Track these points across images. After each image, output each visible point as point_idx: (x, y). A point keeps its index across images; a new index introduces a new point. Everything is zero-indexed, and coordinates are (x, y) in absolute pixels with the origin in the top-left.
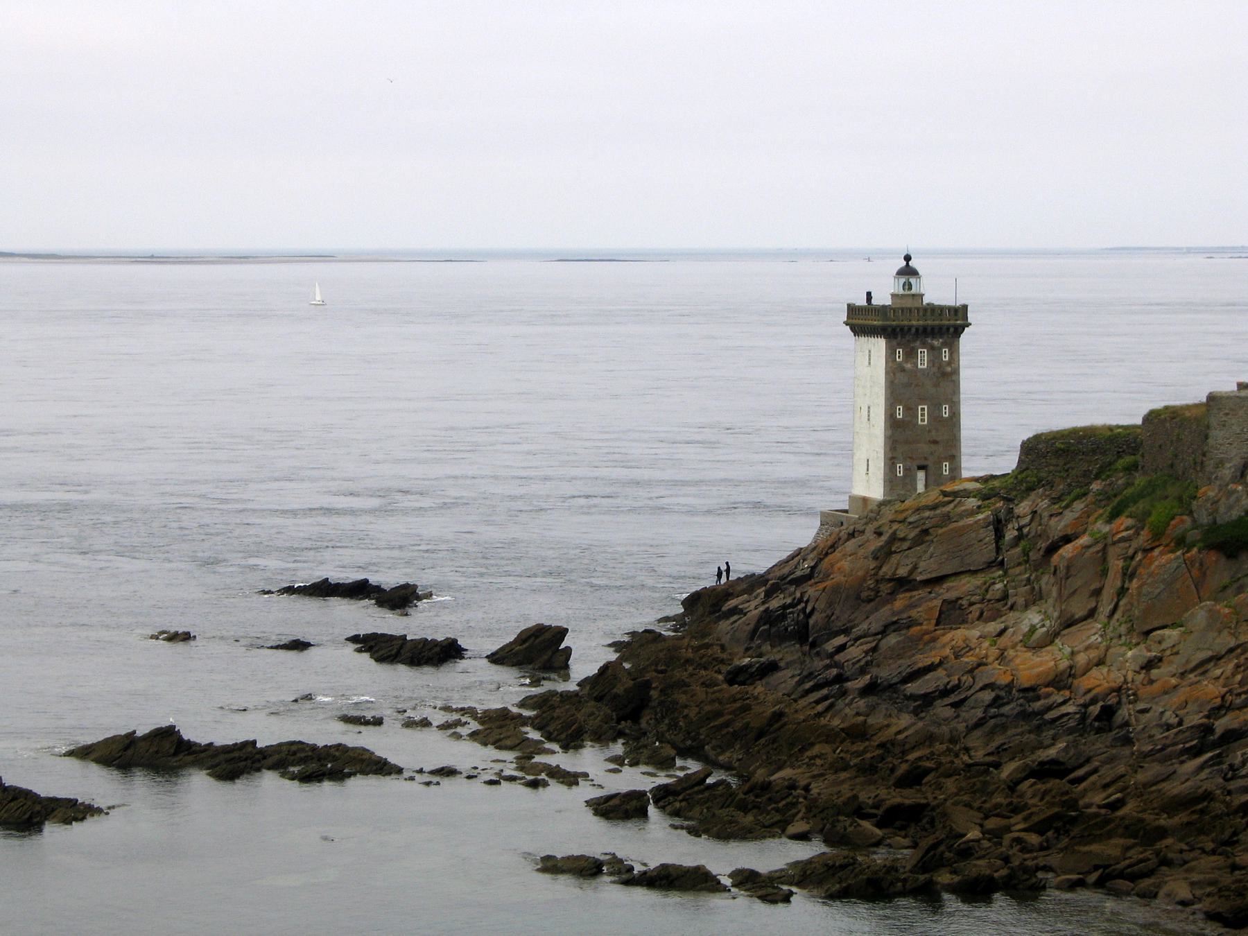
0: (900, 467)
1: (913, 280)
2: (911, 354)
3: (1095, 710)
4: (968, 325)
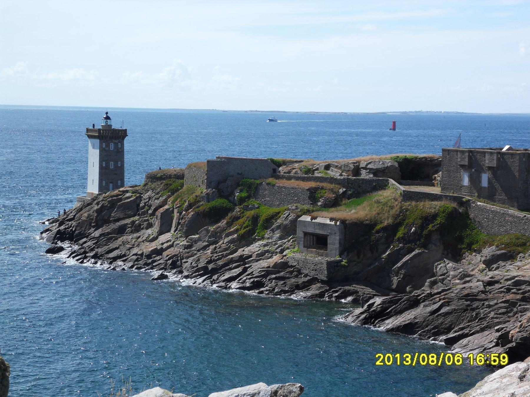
1: (108, 120)
2: (108, 146)
3: (170, 262)
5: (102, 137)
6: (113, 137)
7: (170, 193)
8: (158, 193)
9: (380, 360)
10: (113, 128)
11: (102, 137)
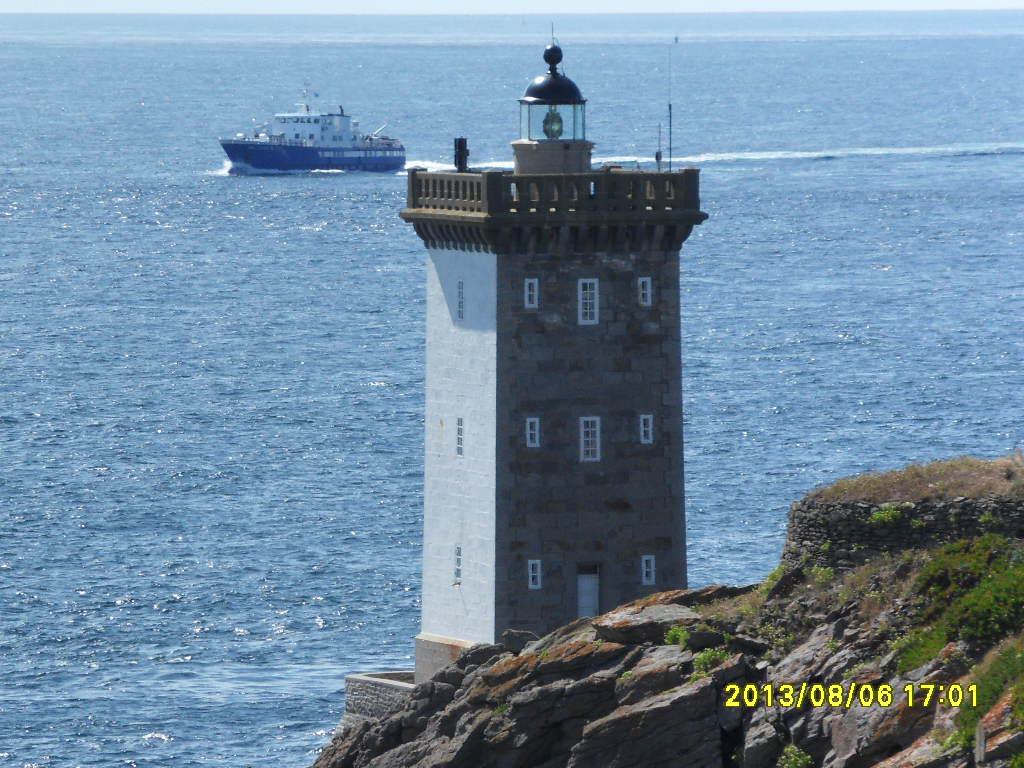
1: (565, 111)
2: (559, 297)
4: (701, 218)
5: (518, 232)
6: (594, 231)
7: (959, 647)
8: (874, 647)
9: (735, 696)
10: (597, 161)
11: (518, 232)
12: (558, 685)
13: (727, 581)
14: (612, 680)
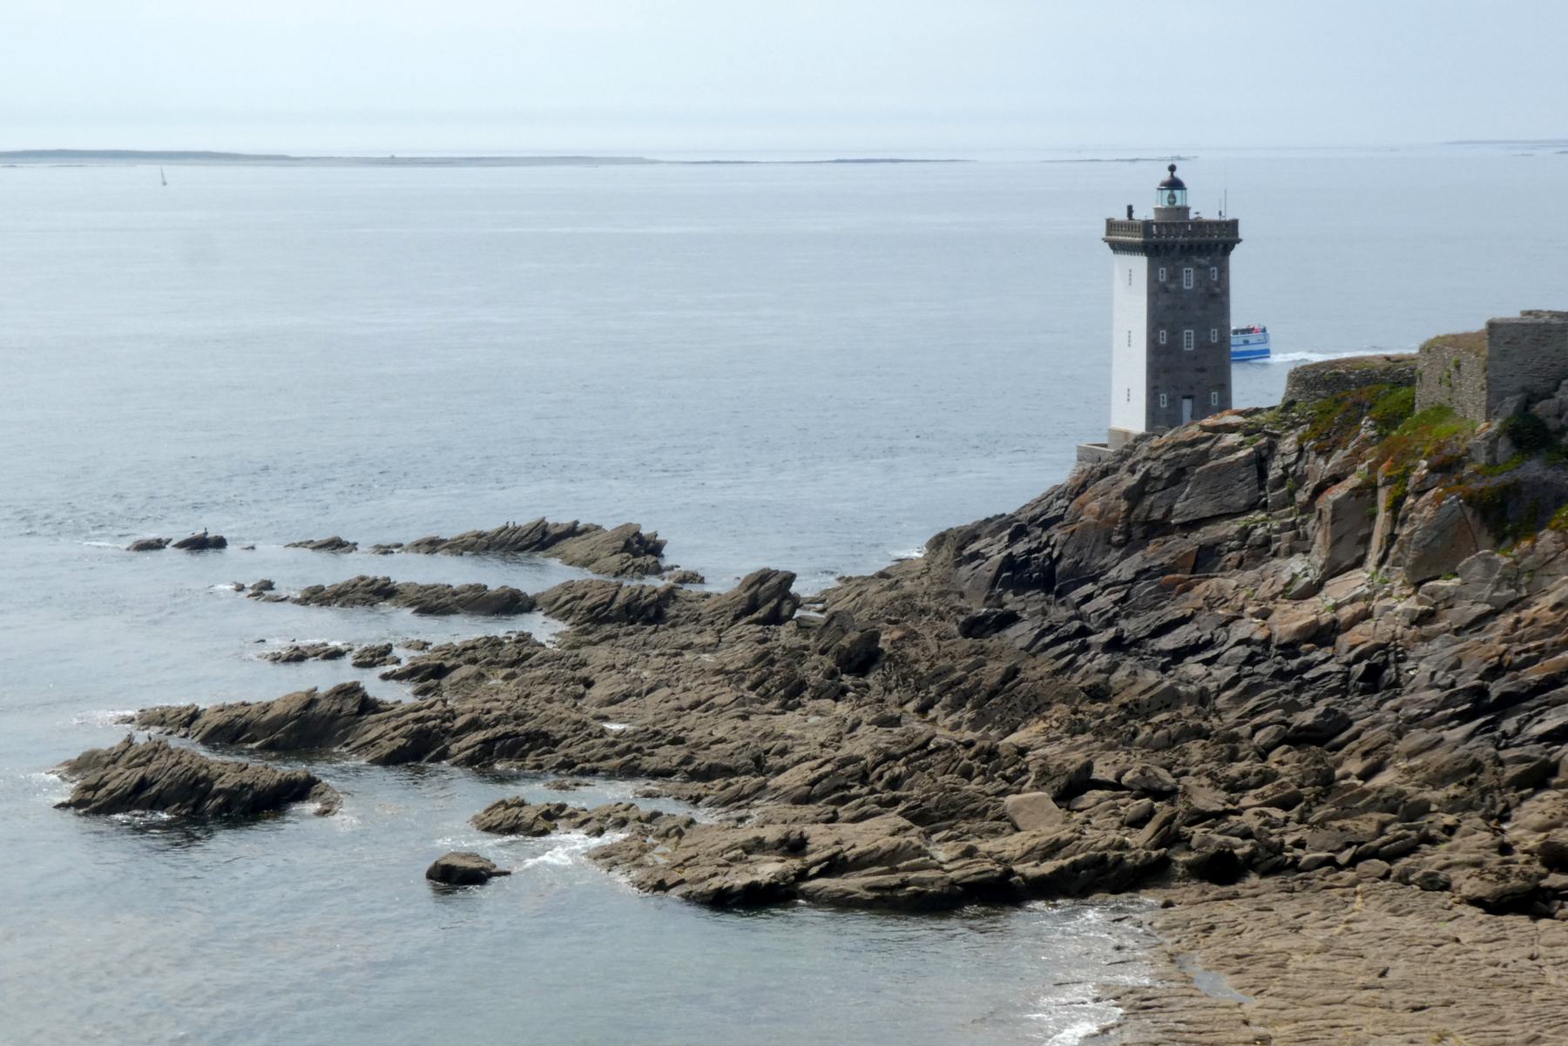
0: (1164, 396)
1: (1177, 193)
2: (1175, 276)
3: (1359, 668)
4: (1239, 241)
10: (1192, 216)
12: (1184, 451)
13: (829, 560)
14: (1208, 450)
